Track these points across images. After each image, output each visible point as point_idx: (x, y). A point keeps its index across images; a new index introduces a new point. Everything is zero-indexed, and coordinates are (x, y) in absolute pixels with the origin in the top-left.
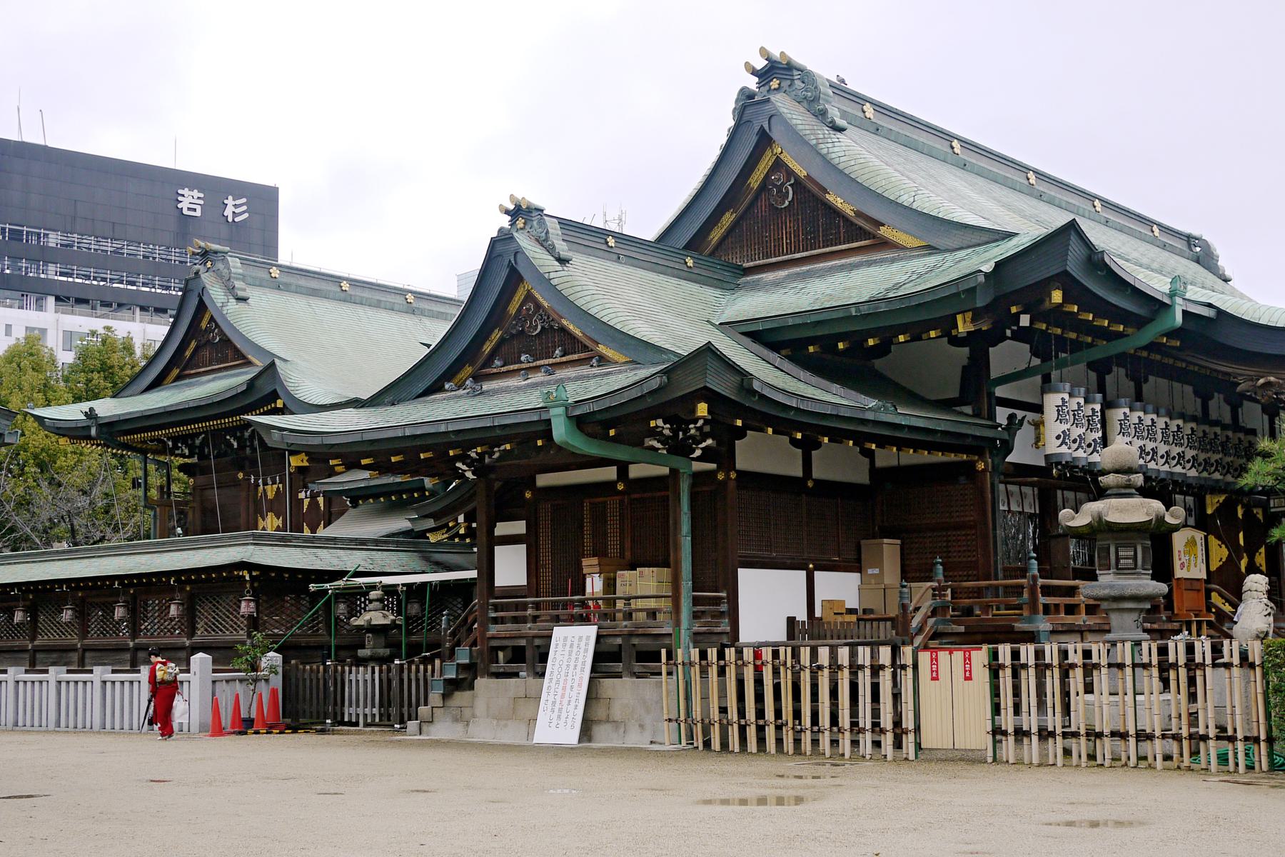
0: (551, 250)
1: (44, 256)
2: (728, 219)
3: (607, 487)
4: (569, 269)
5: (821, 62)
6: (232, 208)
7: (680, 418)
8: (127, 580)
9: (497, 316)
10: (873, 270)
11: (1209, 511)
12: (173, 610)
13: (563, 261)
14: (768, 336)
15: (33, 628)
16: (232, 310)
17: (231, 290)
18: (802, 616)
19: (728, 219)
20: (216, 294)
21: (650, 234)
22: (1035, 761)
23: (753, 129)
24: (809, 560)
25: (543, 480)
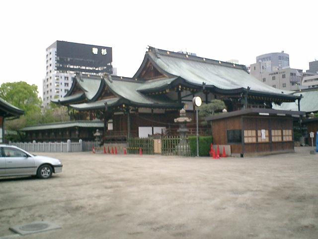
0: (110, 81)
1: (67, 63)
2: (144, 72)
3: (122, 115)
4: (112, 84)
5: (157, 46)
6: (104, 52)
7: (121, 106)
8: (54, 129)
9: (102, 92)
10: (161, 81)
11: (273, 104)
12: (67, 133)
13: (111, 82)
14: (144, 93)
15: (62, 135)
16: (80, 83)
17: (81, 80)
18: (151, 134)
19: (144, 72)
20: (78, 80)
21: (131, 75)
22: (68, 150)
23: (147, 59)
24: (152, 125)
25: (115, 114)
